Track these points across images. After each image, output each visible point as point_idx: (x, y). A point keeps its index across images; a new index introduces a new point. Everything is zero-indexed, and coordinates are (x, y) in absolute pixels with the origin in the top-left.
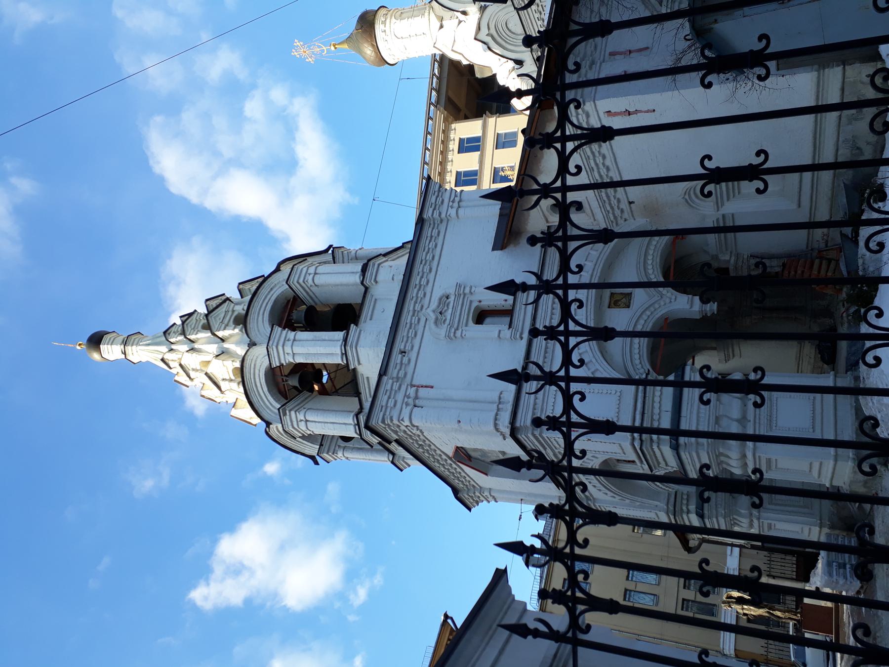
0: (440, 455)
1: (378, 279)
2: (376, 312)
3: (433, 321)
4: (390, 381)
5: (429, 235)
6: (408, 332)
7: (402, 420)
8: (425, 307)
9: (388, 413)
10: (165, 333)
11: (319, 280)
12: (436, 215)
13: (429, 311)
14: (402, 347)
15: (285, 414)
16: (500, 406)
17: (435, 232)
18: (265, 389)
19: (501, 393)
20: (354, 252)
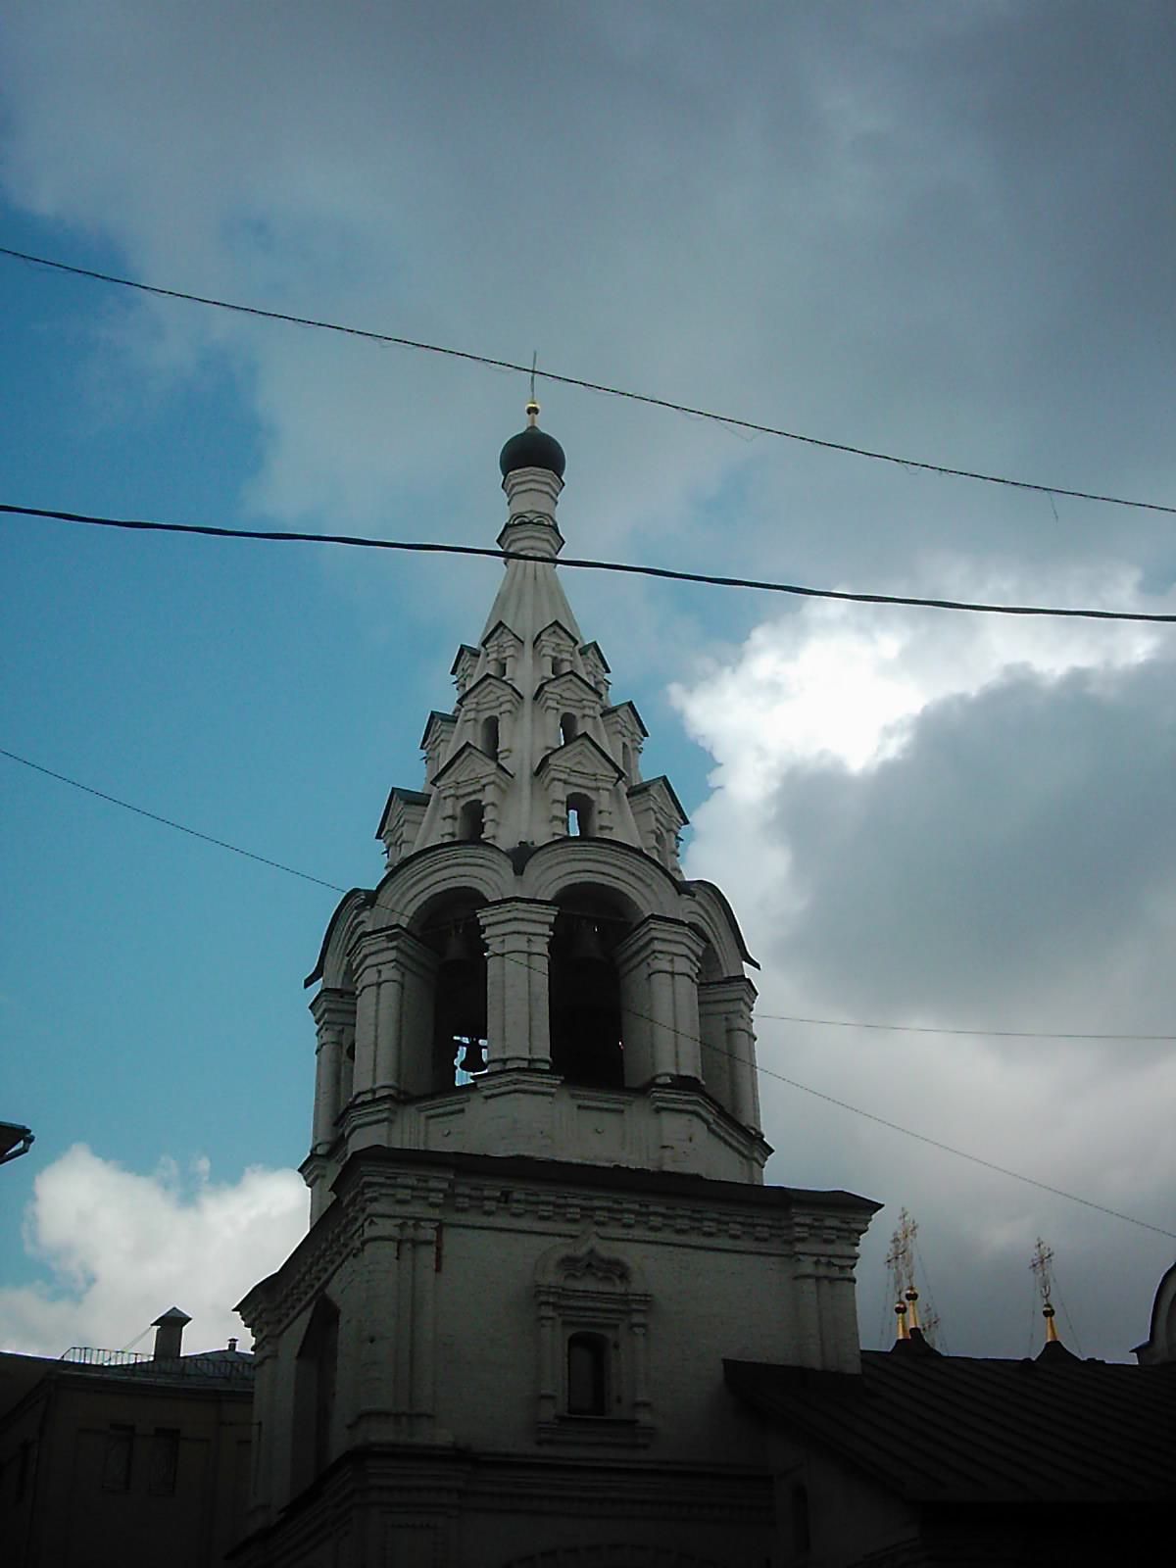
0: (332, 1262)
1: (664, 1115)
2: (595, 1114)
3: (570, 1252)
4: (445, 1186)
5: (756, 1221)
6: (548, 1203)
7: (372, 1222)
8: (601, 1231)
9: (384, 1191)
10: (556, 623)
11: (661, 983)
12: (798, 1232)
13: (594, 1242)
14: (516, 1196)
15: (390, 938)
16: (404, 1420)
17: (765, 1233)
18: (438, 889)
19: (430, 1417)
20: (743, 1025)
